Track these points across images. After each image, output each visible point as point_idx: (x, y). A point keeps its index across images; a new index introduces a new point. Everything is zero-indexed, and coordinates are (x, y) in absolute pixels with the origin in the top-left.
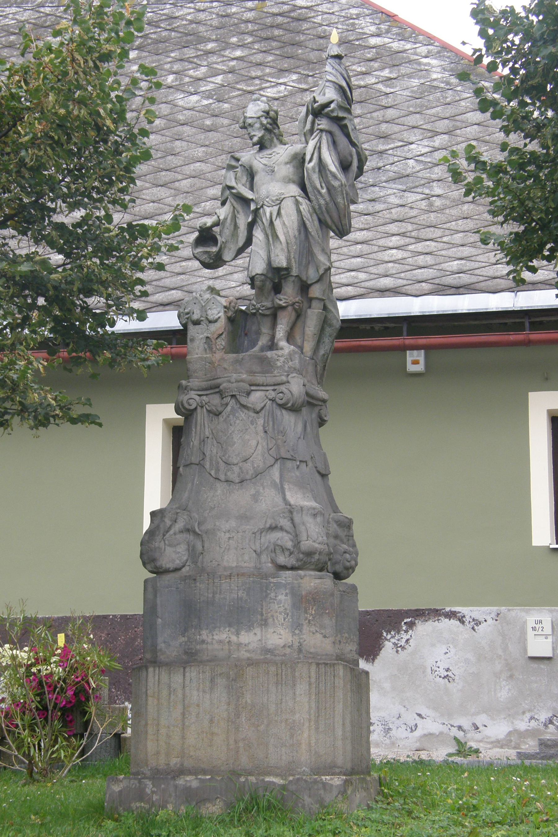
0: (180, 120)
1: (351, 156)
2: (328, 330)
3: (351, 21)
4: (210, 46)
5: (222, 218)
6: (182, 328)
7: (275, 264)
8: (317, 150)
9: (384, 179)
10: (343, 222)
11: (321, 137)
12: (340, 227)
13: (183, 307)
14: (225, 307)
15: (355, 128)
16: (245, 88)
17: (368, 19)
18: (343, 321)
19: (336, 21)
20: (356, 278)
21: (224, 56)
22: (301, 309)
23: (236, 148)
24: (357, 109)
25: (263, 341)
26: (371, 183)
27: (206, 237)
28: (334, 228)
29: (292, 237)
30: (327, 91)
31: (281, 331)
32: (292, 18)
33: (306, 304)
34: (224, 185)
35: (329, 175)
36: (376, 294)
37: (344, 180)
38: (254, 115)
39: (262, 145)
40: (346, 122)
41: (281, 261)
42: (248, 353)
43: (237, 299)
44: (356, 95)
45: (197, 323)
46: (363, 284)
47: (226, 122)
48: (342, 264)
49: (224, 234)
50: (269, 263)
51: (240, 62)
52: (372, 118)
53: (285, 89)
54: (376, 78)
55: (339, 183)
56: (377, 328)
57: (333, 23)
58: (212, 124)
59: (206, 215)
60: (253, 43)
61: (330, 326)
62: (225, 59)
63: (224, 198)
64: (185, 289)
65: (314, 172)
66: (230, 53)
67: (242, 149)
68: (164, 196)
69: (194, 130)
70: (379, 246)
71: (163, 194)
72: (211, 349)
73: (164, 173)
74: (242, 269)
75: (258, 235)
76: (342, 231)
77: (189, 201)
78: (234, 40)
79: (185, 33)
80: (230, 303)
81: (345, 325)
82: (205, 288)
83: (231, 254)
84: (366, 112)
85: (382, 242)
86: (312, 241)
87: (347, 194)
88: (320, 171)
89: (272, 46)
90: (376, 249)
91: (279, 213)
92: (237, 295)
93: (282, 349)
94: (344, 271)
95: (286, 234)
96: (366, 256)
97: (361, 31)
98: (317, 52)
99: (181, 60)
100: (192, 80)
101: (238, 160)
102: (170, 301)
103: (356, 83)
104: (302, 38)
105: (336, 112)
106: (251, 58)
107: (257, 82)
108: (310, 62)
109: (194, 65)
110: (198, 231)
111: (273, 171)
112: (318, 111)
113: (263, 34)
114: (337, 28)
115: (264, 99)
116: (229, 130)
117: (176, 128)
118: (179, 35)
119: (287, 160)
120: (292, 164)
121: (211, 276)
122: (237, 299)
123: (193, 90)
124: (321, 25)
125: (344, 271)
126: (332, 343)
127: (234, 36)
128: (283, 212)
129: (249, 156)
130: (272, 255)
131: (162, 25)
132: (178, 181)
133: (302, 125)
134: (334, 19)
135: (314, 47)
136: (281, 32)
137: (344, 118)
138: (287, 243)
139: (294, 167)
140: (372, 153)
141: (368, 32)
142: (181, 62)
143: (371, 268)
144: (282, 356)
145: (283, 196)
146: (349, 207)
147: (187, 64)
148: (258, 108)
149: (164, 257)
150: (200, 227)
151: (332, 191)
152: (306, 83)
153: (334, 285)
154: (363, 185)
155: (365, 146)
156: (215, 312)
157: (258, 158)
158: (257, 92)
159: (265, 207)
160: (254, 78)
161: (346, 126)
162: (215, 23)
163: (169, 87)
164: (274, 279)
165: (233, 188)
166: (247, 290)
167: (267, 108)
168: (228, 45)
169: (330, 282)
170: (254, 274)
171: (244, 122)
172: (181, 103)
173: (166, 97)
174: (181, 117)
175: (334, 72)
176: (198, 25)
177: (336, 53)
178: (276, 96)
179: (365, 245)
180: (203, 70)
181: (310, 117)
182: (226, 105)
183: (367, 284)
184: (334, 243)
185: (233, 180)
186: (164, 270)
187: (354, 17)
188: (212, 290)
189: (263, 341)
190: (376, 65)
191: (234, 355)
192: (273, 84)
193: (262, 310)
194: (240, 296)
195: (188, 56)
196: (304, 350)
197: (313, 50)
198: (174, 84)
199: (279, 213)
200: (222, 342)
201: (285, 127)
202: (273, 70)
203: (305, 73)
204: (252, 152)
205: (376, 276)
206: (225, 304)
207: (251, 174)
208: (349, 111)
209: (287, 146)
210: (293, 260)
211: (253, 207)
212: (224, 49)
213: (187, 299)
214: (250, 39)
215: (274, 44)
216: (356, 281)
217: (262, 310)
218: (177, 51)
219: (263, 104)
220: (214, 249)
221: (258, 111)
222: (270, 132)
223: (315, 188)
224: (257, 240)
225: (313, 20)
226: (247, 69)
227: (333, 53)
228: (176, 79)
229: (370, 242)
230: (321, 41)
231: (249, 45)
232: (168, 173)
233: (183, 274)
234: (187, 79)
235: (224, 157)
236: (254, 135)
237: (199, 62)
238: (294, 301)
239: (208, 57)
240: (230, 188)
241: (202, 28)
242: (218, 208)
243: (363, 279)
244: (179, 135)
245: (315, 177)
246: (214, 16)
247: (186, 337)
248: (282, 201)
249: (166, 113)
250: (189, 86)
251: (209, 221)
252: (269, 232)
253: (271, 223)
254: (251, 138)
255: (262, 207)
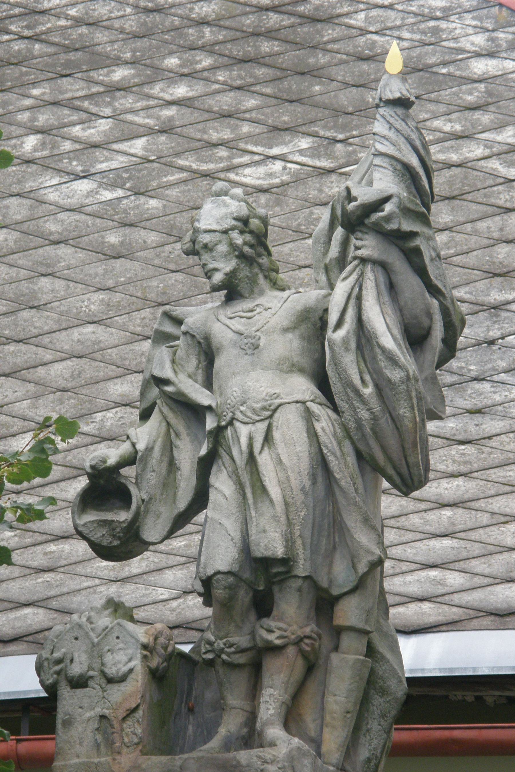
0: (51, 233)
1: (429, 315)
2: (378, 702)
3: (432, 23)
4: (119, 74)
5: (141, 446)
6: (46, 695)
7: (259, 552)
8: (353, 301)
9: (503, 364)
10: (412, 460)
11: (362, 275)
12: (404, 470)
13: (49, 647)
14: (145, 647)
15: (438, 256)
16: (194, 166)
17: (468, 19)
18: (411, 681)
19: (398, 23)
20: (441, 583)
21: (149, 97)
22: (316, 652)
23: (175, 294)
24: (442, 214)
25: (230, 725)
26: (473, 374)
27: (105, 488)
28: (391, 471)
29: (296, 490)
30: (377, 175)
31: (271, 703)
32: (301, 16)
33: (327, 642)
34: (147, 375)
35: (380, 357)
36: (488, 621)
37: (412, 368)
38: (214, 227)
39: (232, 291)
40: (418, 242)
41: (271, 542)
42: (195, 754)
43: (171, 628)
44: (441, 182)
45: (79, 683)
46: (456, 598)
47: (152, 238)
48: (409, 552)
49: (145, 483)
50: (246, 547)
51: (185, 110)
52: (476, 233)
53: (285, 168)
54: (486, 146)
55: (403, 374)
56: (490, 700)
57: (391, 29)
58: (122, 243)
59: (104, 439)
60: (213, 68)
61: (383, 692)
62: (152, 103)
63: (146, 405)
64: (54, 604)
65: (347, 349)
66: (162, 90)
67: (186, 298)
68: (11, 397)
69: (81, 255)
70: (493, 513)
71: (9, 393)
72: (110, 743)
73: (12, 347)
74: (183, 559)
75: (222, 484)
76: (409, 481)
77: (68, 409)
78: (172, 62)
79: (64, 46)
80: (156, 639)
81: (416, 691)
82: (99, 602)
83: (159, 527)
84: (462, 219)
85: (498, 504)
86: (340, 499)
87: (420, 399)
88: (359, 347)
89: (255, 77)
90: (485, 519)
91: (268, 439)
92: (173, 618)
93: (272, 744)
94: (414, 566)
95: (284, 485)
96: (462, 535)
97: (452, 44)
98: (354, 90)
99: (55, 104)
100: (78, 146)
101: (178, 322)
102: (20, 631)
103: (441, 157)
104: (323, 59)
105: (396, 221)
106: (210, 102)
107: (223, 152)
108: (339, 112)
109: (84, 116)
110: (88, 474)
111: (256, 347)
112: (356, 220)
113: (237, 50)
114: (399, 38)
115: (238, 191)
116: (158, 256)
117: (41, 251)
118: (51, 50)
119: (286, 323)
120: (297, 332)
121: (112, 575)
122: (171, 628)
123: (80, 168)
124: (364, 32)
125: (414, 566)
126: (388, 732)
127: (171, 53)
128: (276, 435)
129: (202, 313)
130: (253, 531)
131: (13, 28)
132: (45, 364)
133: (320, 248)
134: (393, 18)
135: (349, 79)
136: (276, 47)
137: (413, 235)
138: (286, 504)
139: (302, 338)
140: (476, 308)
141: (468, 47)
142: (55, 109)
143: (474, 563)
144: (272, 762)
145: (278, 401)
146: (424, 426)
147: (66, 111)
148: (223, 211)
149: (9, 534)
150: (92, 467)
151: (387, 391)
152: (330, 156)
153: (390, 599)
154: (455, 378)
155: (459, 293)
156: (121, 657)
157: (222, 318)
158: (222, 175)
159: (237, 424)
160: (216, 145)
161: (417, 251)
162: (131, 24)
163: (28, 162)
164: (255, 584)
165: (167, 382)
166: (194, 608)
167: (244, 211)
168: (158, 74)
169: (382, 592)
170: (210, 572)
171: (194, 242)
172: (52, 196)
173: (19, 182)
174: (52, 227)
175: (391, 134)
176: (92, 29)
177: (397, 95)
178: (264, 183)
179: (460, 511)
180: (104, 125)
181: (339, 232)
182: (153, 203)
183: (467, 598)
184: (390, 503)
185: (168, 364)
186: (10, 563)
187: (438, 14)
188: (115, 607)
189: (230, 725)
190: (485, 118)
191: (164, 759)
192: (257, 158)
193: (228, 654)
194: (180, 620)
195: (69, 95)
196: (324, 749)
197: (347, 85)
198: (38, 154)
199: (268, 439)
200: (136, 729)
201: (283, 250)
202: (258, 129)
203: (328, 134)
204: (209, 305)
205: (486, 581)
206: (144, 640)
207: (207, 352)
208: (424, 219)
209: (287, 293)
210: (299, 542)
211: (210, 423)
212: (151, 82)
213: (58, 628)
214: (207, 62)
215: (261, 72)
216: (441, 590)
217: (228, 654)
218: (46, 85)
219: (236, 203)
220: (123, 516)
221: (225, 216)
222: (250, 262)
223: (348, 384)
224: (220, 497)
225: (347, 20)
226: (200, 126)
227: (389, 96)
228: (43, 144)
229: (472, 504)
230: (365, 66)
231: (205, 74)
232: (22, 347)
233: (50, 570)
234: (67, 146)
235: (146, 313)
236: (216, 270)
237: (94, 109)
238: (300, 633)
239: (114, 98)
240: (161, 382)
241: (100, 36)
242: (132, 424)
243: (456, 587)
244: (48, 265)
245: (350, 362)
246: (129, 10)
247: (54, 718)
248: (275, 411)
249: (19, 217)
250: (71, 160)
251: (112, 454)
252: (246, 478)
253: (251, 459)
254: (209, 274)
255: (231, 423)
